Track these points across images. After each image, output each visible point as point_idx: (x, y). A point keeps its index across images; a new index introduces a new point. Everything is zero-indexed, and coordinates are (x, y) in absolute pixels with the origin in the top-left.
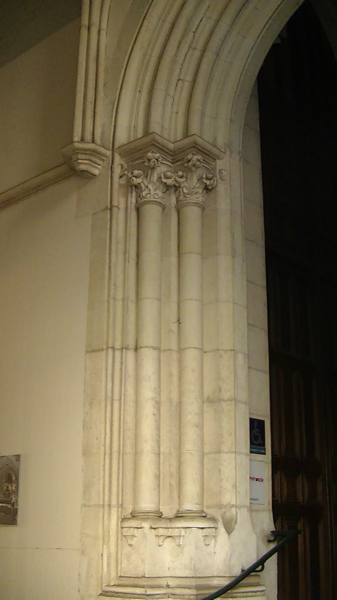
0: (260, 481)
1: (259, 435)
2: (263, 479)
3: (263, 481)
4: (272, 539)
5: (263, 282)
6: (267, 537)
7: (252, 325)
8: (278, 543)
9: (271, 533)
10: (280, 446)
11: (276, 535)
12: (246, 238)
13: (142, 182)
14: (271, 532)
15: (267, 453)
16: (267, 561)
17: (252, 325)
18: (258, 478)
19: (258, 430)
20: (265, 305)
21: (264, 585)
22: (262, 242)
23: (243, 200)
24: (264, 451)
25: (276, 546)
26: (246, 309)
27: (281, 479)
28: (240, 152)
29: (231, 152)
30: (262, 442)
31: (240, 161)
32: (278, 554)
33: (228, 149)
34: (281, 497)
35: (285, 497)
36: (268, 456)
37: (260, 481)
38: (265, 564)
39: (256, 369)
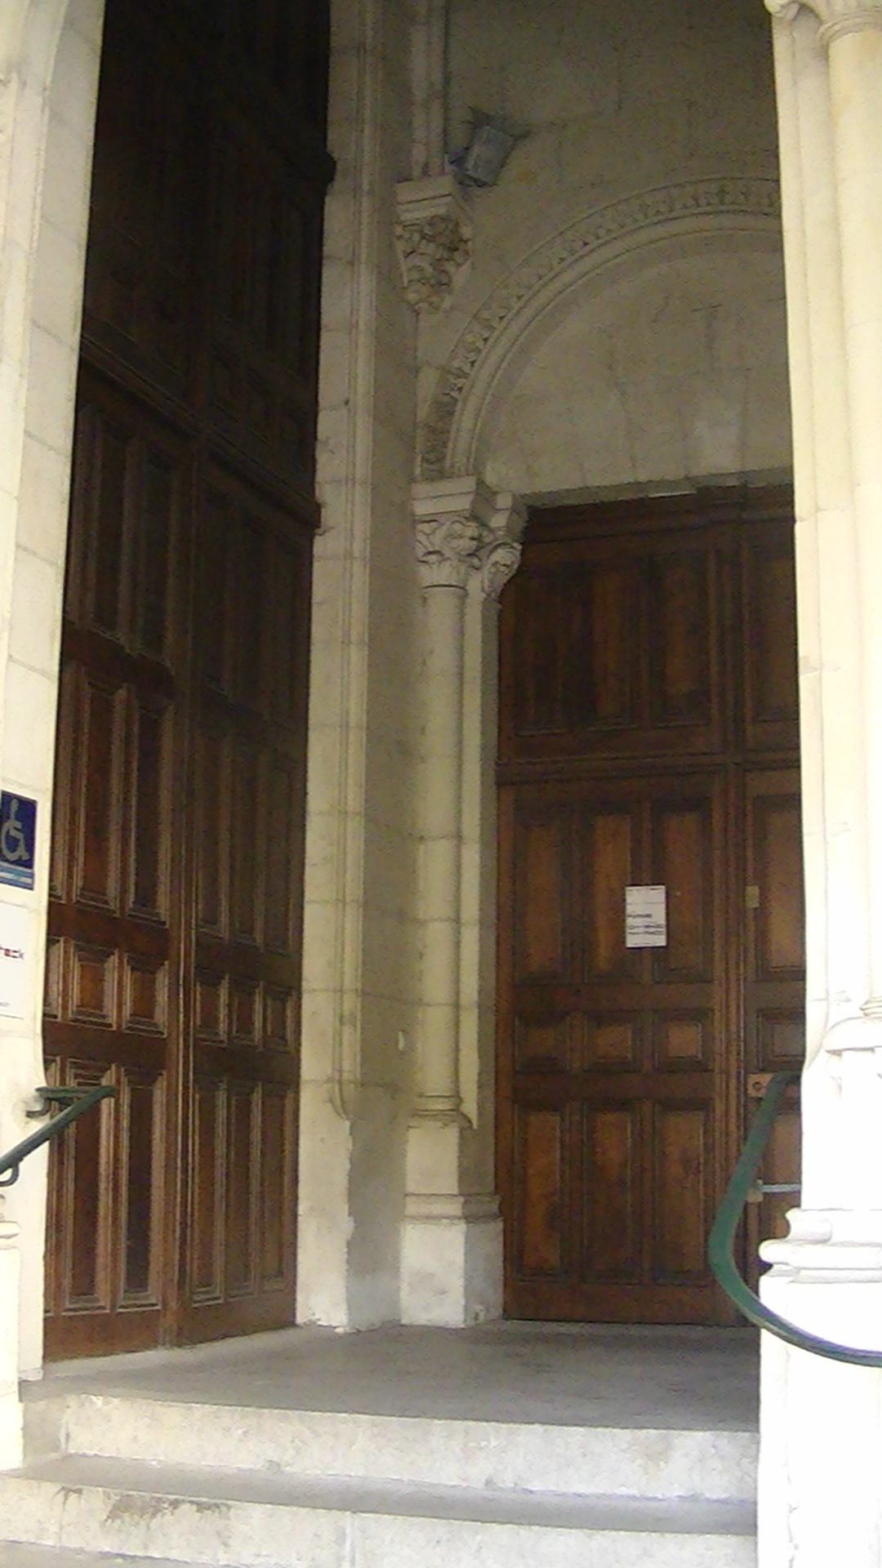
0: (14, 957)
1: (20, 836)
2: (22, 952)
3: (24, 956)
4: (38, 1108)
5: (65, 442)
6: (25, 1102)
7: (26, 549)
8: (52, 1117)
9: (37, 1094)
10: (70, 876)
11: (50, 1099)
12: (34, 322)
13: (99, 1084)
14: (38, 1090)
15: (36, 886)
16: (26, 1159)
17: (26, 549)
18: (12, 948)
19: (19, 825)
20: (63, 502)
21: (15, 1222)
22: (73, 338)
23: (37, 223)
24: (29, 881)
25: (44, 1127)
26: (15, 501)
27: (66, 959)
28: (45, 89)
29: (23, 84)
30: (26, 857)
31: (43, 111)
32: (51, 1144)
33: (14, 75)
34: (65, 1008)
35: (75, 1009)
36: (39, 896)
37: (14, 957)
38: (22, 1165)
39: (23, 664)
